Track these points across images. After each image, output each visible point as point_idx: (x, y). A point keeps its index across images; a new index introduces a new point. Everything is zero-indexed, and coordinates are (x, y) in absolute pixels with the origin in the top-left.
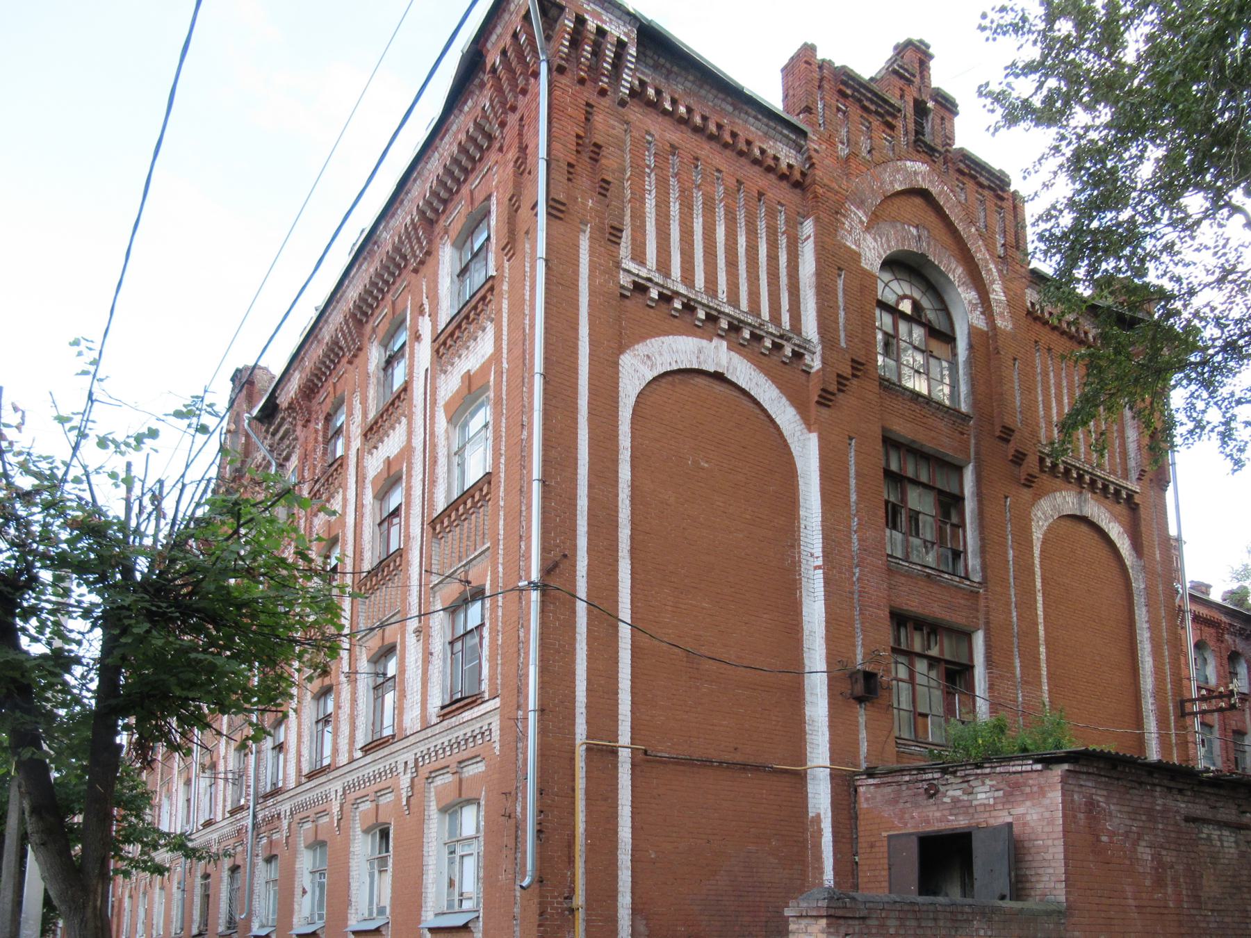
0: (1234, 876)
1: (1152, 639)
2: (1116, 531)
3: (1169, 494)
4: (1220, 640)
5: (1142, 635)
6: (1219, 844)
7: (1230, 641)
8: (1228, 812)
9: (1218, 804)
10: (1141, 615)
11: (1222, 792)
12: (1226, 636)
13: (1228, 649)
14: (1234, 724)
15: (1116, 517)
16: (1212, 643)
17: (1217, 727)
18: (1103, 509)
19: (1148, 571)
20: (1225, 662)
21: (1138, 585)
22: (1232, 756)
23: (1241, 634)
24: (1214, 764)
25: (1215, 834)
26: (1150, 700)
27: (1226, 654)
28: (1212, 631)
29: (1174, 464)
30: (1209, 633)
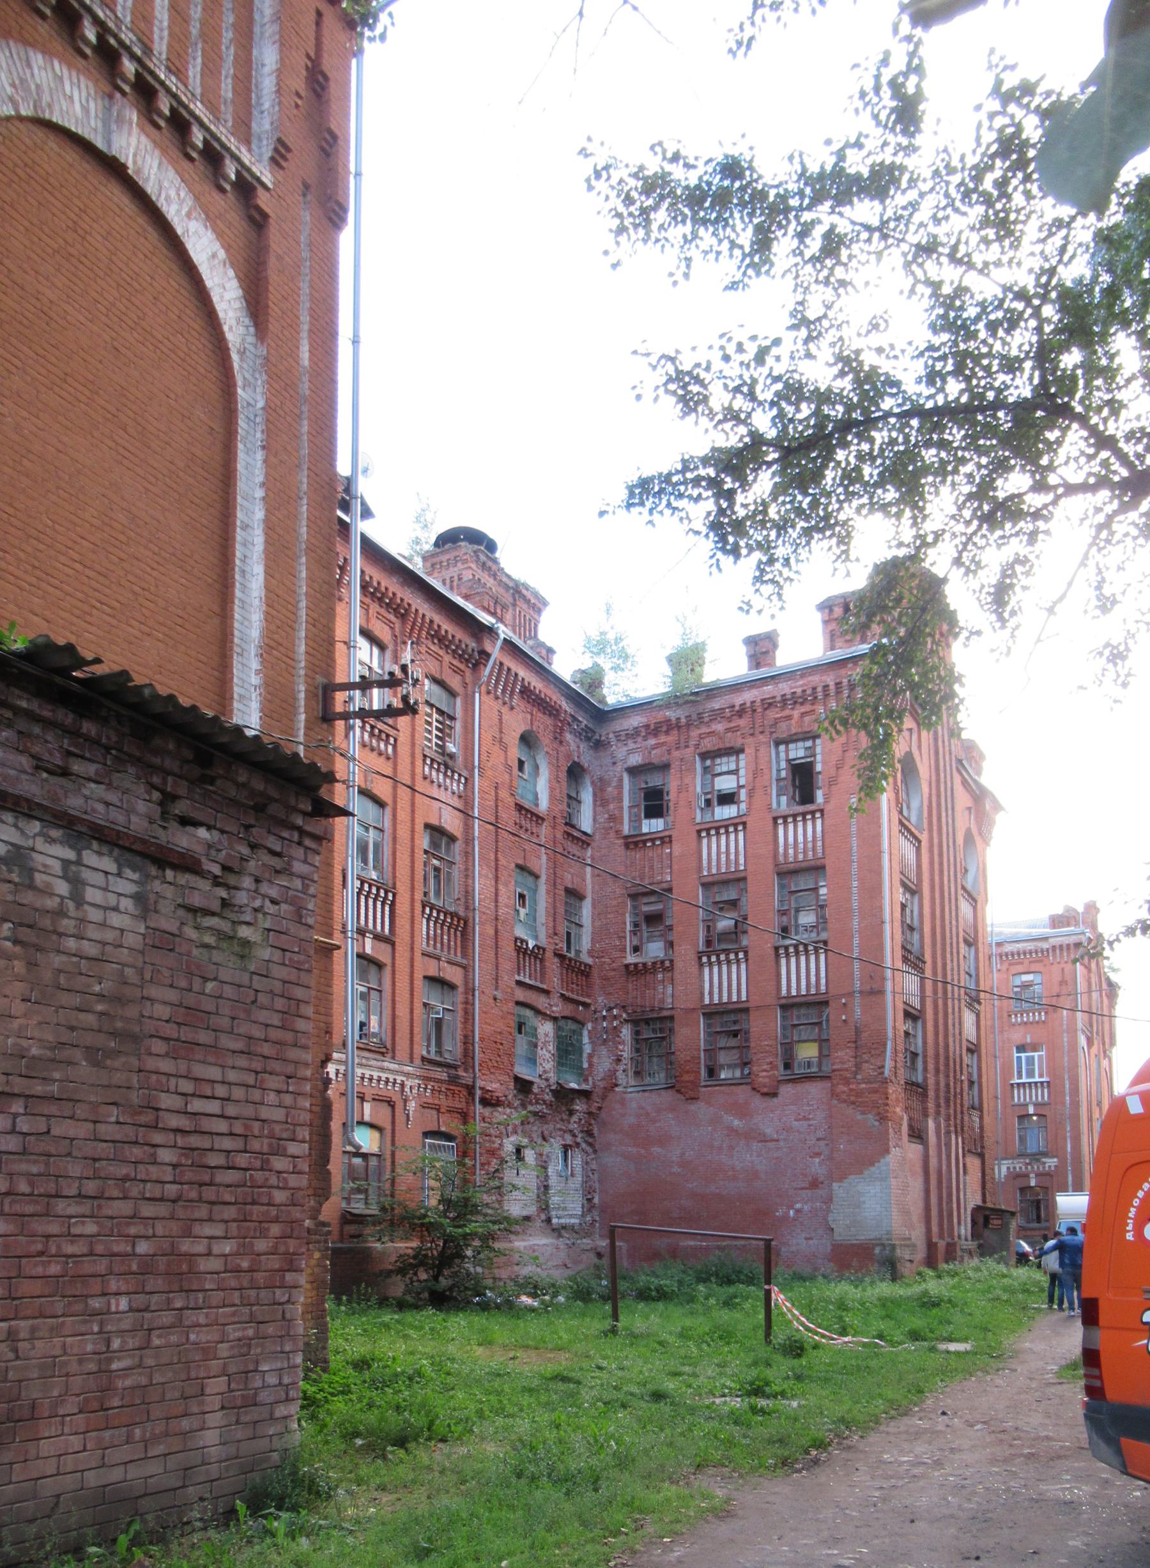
0: (118, 1000)
1: (269, 527)
2: (204, 246)
3: (345, 238)
4: (558, 739)
5: (249, 513)
6: (62, 888)
7: (573, 747)
8: (131, 807)
9: (77, 767)
10: (251, 467)
11: (89, 728)
12: (568, 737)
13: (569, 756)
14: (569, 880)
15: (212, 220)
16: (545, 739)
17: (543, 878)
18: (171, 173)
19: (279, 376)
20: (563, 775)
21: (251, 395)
22: (562, 929)
23: (588, 739)
24: (536, 938)
25: (51, 854)
26: (255, 664)
27: (565, 765)
28: (549, 721)
29: (358, 174)
30: (543, 725)
